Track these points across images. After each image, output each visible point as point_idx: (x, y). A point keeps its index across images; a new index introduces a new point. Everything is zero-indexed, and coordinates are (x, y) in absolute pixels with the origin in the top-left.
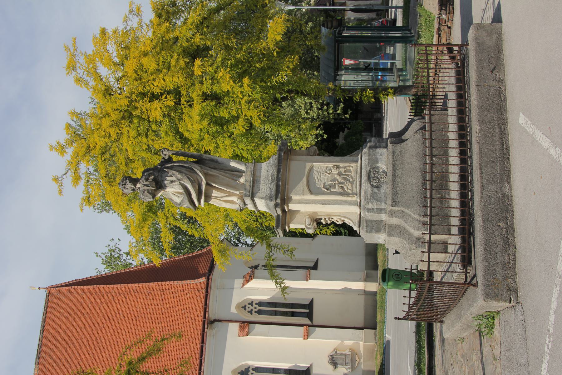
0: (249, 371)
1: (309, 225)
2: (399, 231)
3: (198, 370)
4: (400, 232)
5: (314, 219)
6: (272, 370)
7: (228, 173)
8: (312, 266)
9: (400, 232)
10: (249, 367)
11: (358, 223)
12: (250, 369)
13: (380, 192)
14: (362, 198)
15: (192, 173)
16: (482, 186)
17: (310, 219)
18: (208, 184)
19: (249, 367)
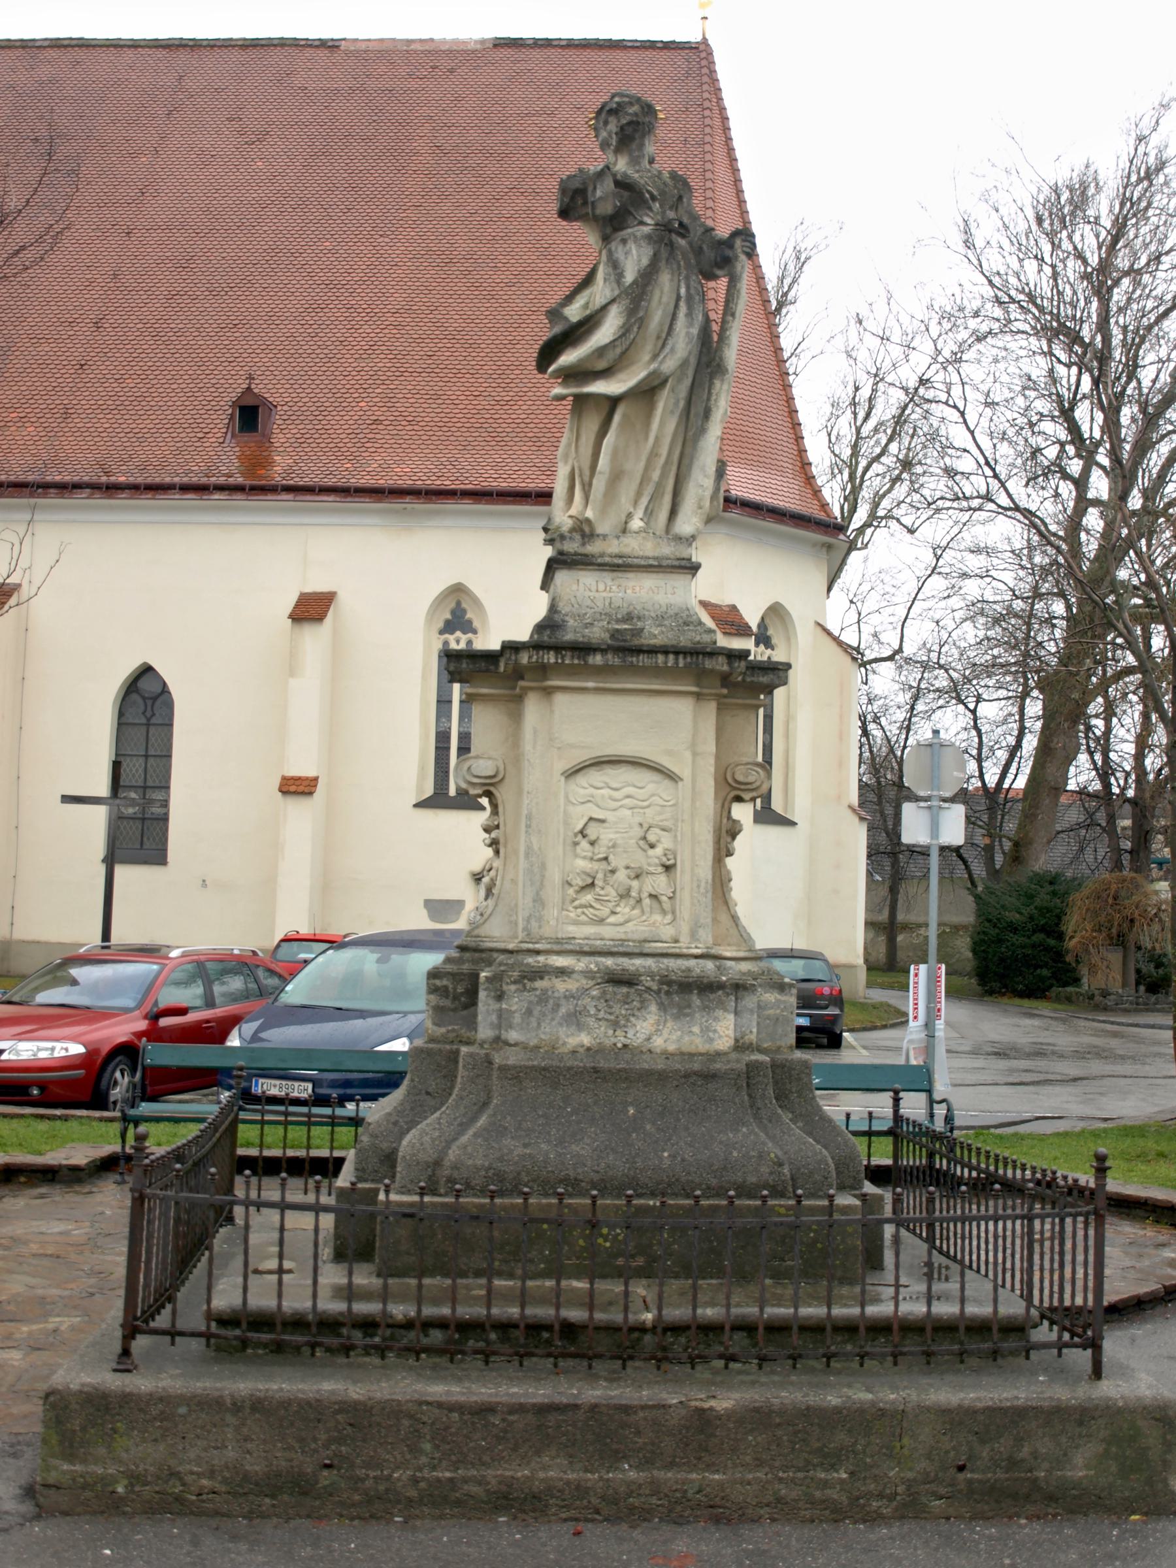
0: (464, 633)
1: (469, 768)
2: (430, 1090)
3: (462, 486)
4: (428, 1093)
5: (492, 789)
6: (447, 699)
7: (663, 476)
8: (773, 807)
9: (428, 1093)
10: (475, 632)
11: (473, 944)
12: (470, 635)
13: (561, 1024)
14: (368, 959)
15: (655, 345)
16: (486, 1409)
17: (491, 773)
18: (614, 402)
19: (475, 632)
